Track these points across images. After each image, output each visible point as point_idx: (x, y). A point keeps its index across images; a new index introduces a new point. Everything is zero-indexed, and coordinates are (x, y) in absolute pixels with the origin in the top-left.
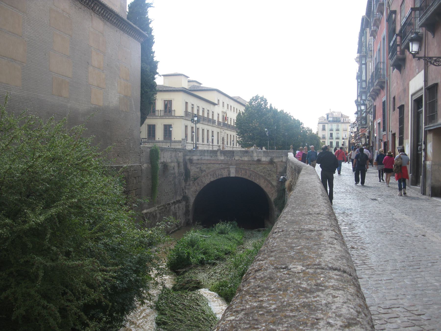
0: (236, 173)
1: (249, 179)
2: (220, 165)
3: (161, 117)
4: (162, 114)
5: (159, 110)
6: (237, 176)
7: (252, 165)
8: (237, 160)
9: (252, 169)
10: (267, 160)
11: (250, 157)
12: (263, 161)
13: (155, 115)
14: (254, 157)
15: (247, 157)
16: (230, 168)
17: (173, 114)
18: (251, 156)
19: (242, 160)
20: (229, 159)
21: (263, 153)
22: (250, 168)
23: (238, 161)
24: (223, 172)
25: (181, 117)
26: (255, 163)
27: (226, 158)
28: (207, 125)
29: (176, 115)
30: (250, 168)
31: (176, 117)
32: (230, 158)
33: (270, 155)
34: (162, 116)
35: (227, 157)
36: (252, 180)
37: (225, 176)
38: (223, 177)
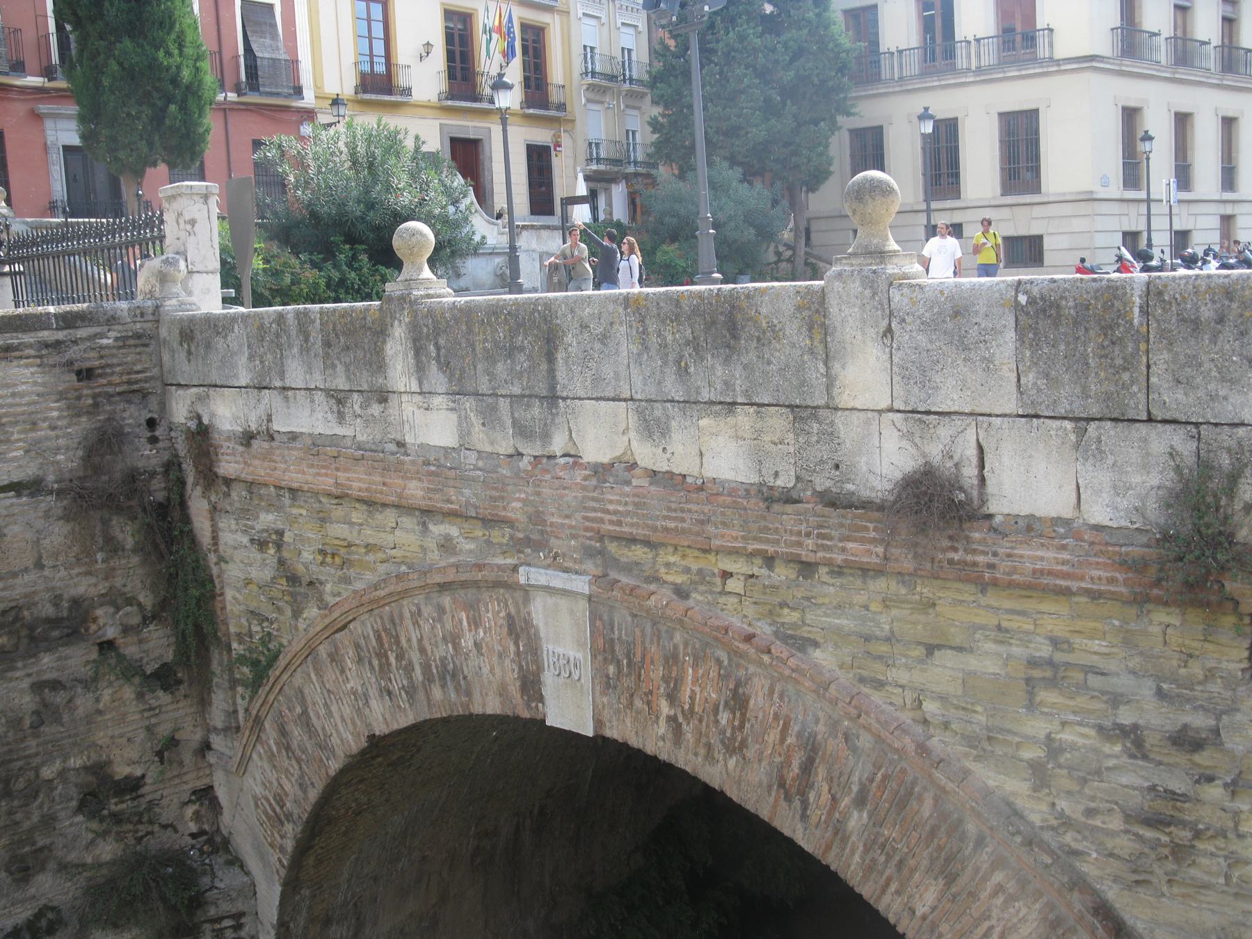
0: (607, 684)
1: (788, 823)
2: (438, 529)
3: (983, 75)
4: (989, 58)
5: (970, 38)
6: (621, 730)
7: (828, 588)
8: (601, 471)
9: (823, 657)
10: (1099, 512)
11: (778, 422)
12: (1030, 527)
13: (952, 69)
14: (848, 428)
15: (745, 418)
16: (526, 591)
17: (1042, 51)
18: (801, 413)
19: (671, 481)
20: (505, 445)
21: (1006, 346)
22: (804, 644)
23: (614, 497)
24: (467, 642)
25: (1088, 62)
26: (870, 554)
27: (480, 438)
28: (1218, 86)
29: (1060, 53)
30: (804, 644)
31: (1058, 62)
32: (522, 431)
33: (1172, 399)
34: (990, 69)
35: (489, 417)
36: (832, 860)
37: (493, 706)
38: (477, 709)
